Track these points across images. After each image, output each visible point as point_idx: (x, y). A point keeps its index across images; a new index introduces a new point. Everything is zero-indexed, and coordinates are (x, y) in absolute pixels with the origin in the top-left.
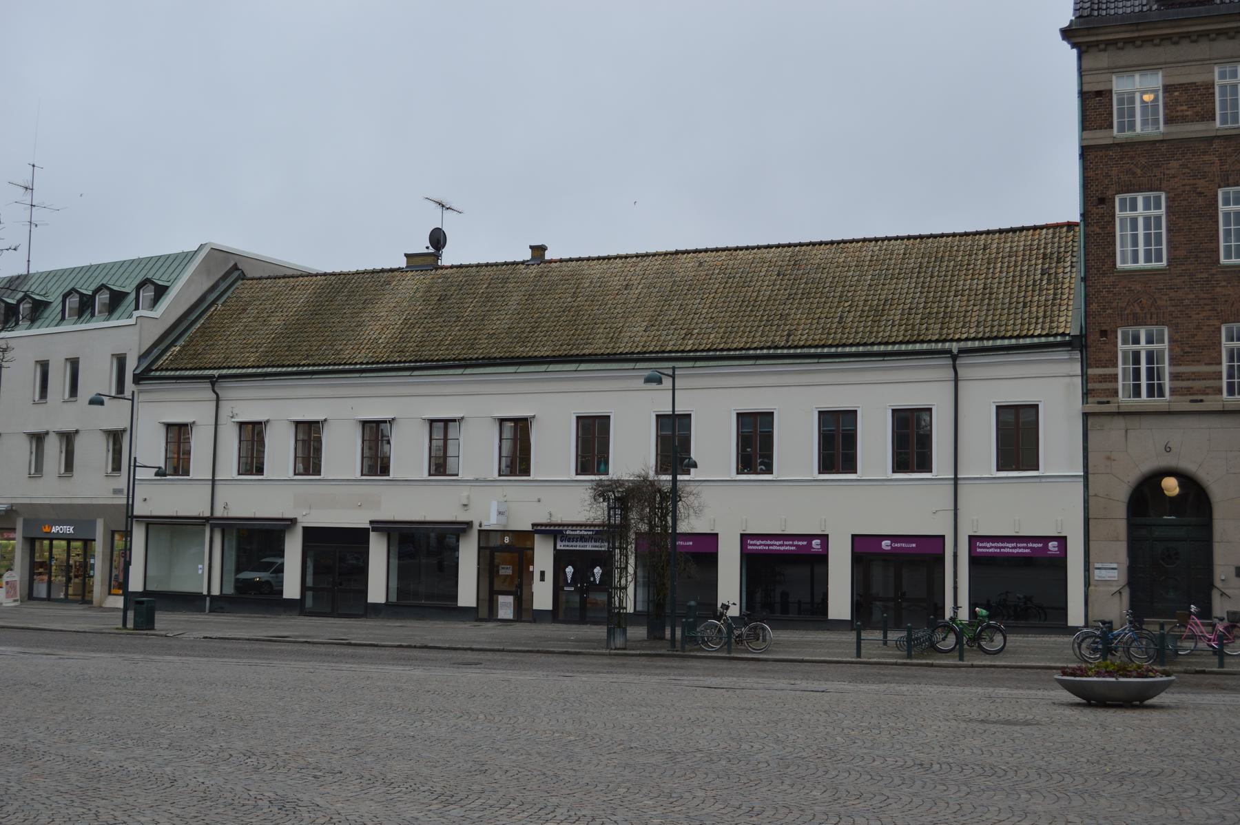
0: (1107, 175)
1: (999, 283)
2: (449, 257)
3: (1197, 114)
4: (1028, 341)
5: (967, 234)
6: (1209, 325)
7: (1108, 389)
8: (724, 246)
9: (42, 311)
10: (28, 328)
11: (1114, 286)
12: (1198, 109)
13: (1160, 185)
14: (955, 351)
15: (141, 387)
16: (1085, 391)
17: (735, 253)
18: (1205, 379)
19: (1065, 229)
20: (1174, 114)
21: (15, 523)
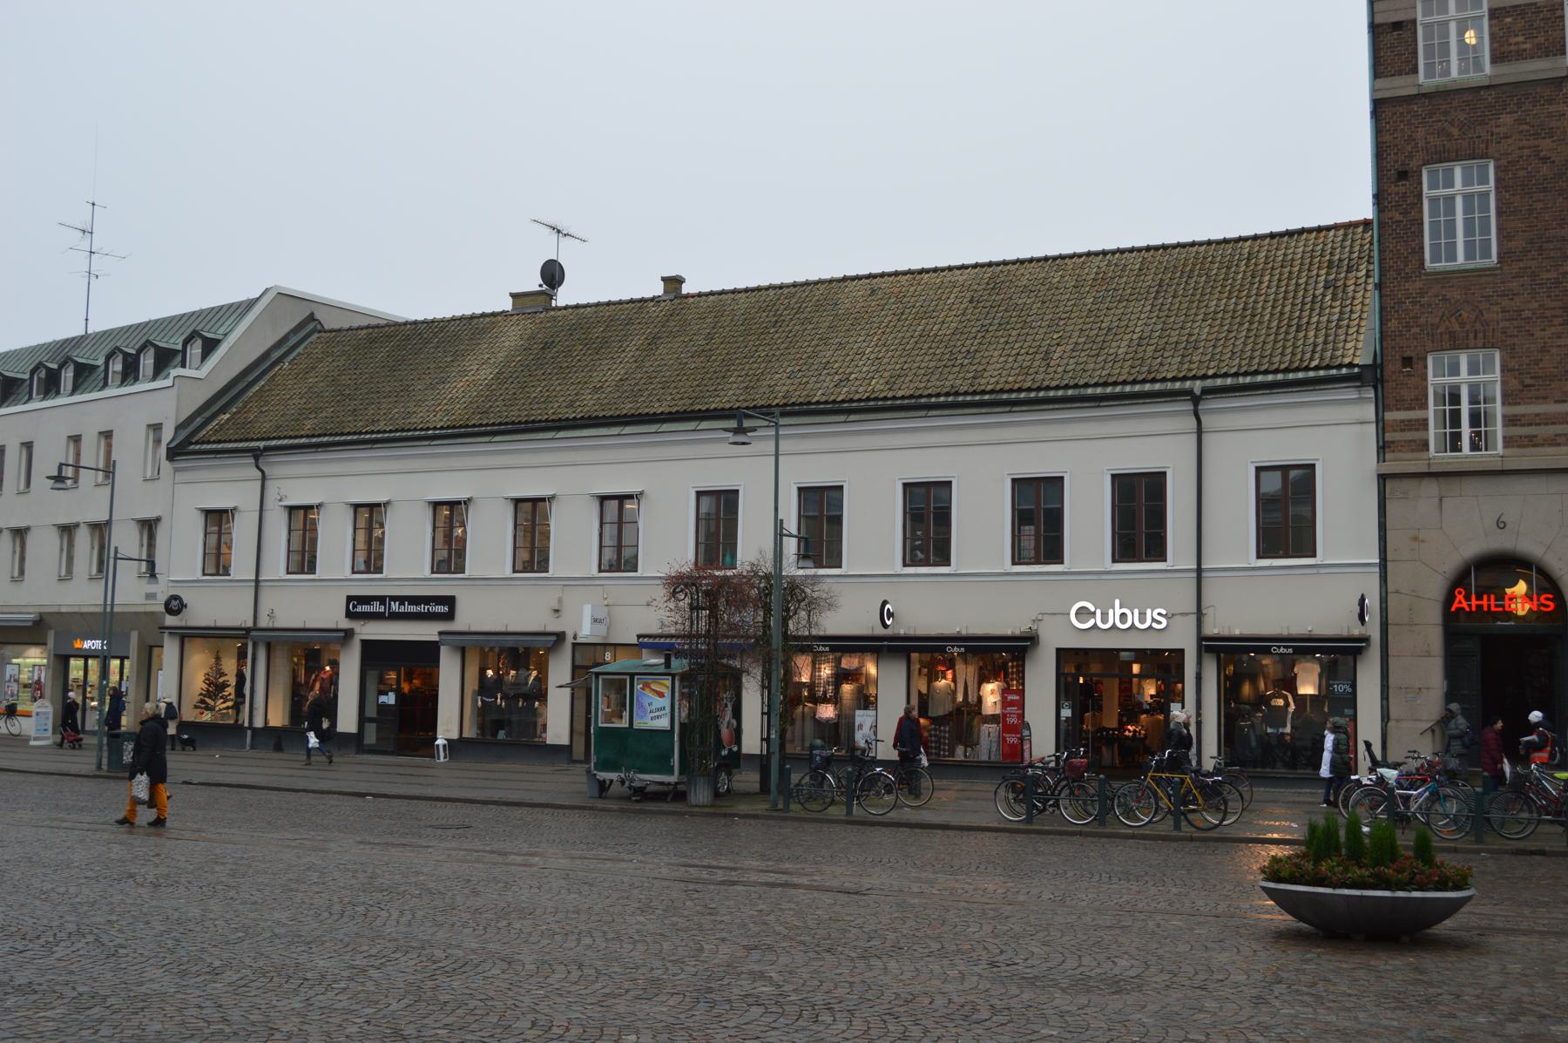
0: (1411, 139)
1: (1265, 301)
2: (565, 296)
3: (1539, 47)
4: (1301, 375)
5: (1226, 241)
6: (1558, 346)
7: (1415, 441)
8: (905, 268)
9: (87, 377)
10: (43, 399)
11: (1422, 293)
12: (1541, 39)
13: (1487, 148)
14: (1197, 391)
15: (178, 465)
16: (1381, 444)
17: (918, 277)
18: (1554, 423)
19: (1360, 229)
20: (1506, 48)
21: (46, 637)
